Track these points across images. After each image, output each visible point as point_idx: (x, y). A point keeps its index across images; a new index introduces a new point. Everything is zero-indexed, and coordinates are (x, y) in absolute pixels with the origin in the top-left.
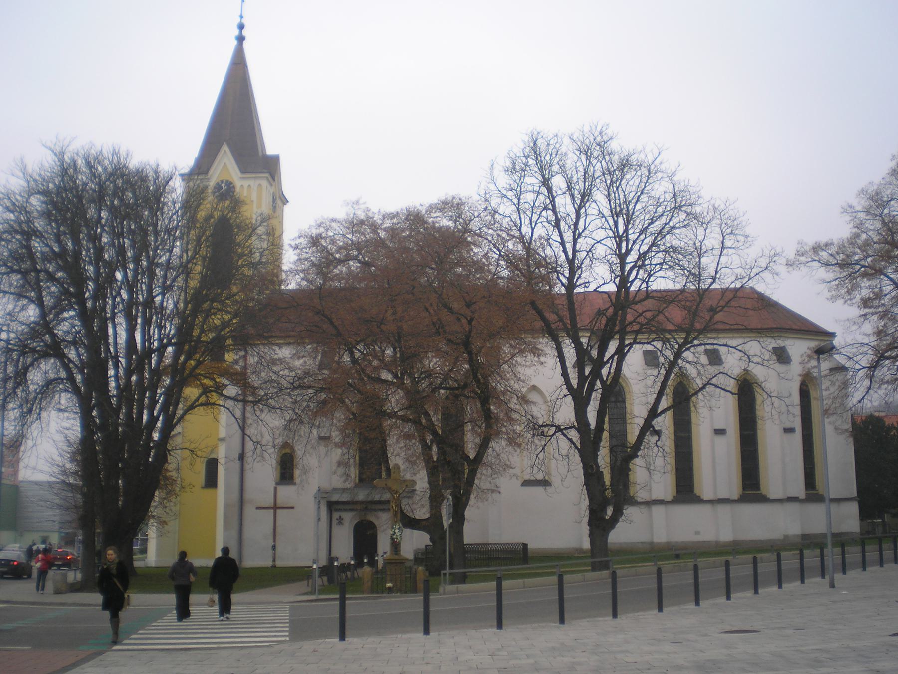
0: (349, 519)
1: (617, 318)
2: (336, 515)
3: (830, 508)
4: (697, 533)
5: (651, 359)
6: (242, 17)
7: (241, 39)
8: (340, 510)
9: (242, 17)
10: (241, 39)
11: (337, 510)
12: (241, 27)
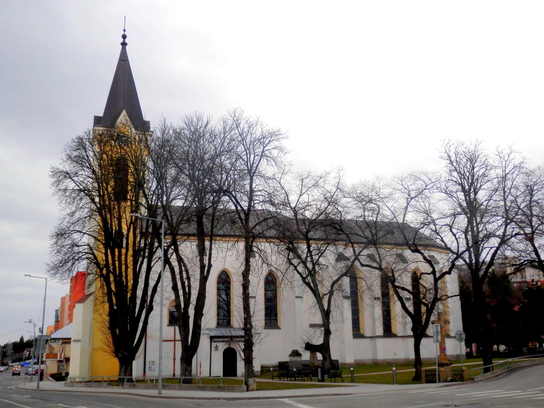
0: (222, 346)
1: (127, 180)
2: (214, 345)
3: (159, 373)
4: (395, 354)
5: (340, 257)
6: (124, 31)
7: (124, 44)
8: (216, 342)
9: (124, 31)
10: (124, 44)
11: (214, 342)
12: (124, 37)
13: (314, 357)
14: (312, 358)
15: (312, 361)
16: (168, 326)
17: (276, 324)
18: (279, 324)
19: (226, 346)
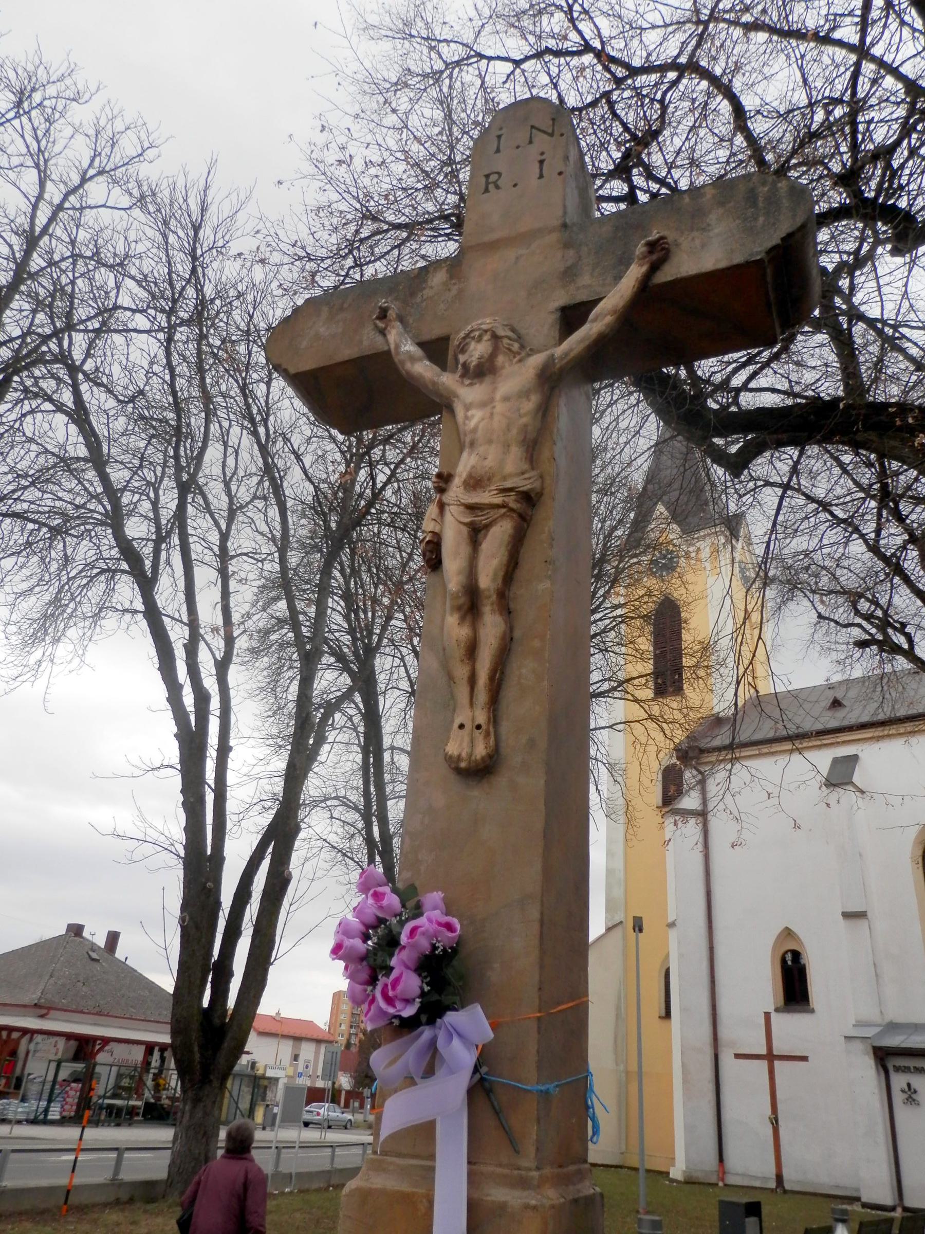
2: (899, 1081)
8: (906, 1070)
11: (897, 1069)
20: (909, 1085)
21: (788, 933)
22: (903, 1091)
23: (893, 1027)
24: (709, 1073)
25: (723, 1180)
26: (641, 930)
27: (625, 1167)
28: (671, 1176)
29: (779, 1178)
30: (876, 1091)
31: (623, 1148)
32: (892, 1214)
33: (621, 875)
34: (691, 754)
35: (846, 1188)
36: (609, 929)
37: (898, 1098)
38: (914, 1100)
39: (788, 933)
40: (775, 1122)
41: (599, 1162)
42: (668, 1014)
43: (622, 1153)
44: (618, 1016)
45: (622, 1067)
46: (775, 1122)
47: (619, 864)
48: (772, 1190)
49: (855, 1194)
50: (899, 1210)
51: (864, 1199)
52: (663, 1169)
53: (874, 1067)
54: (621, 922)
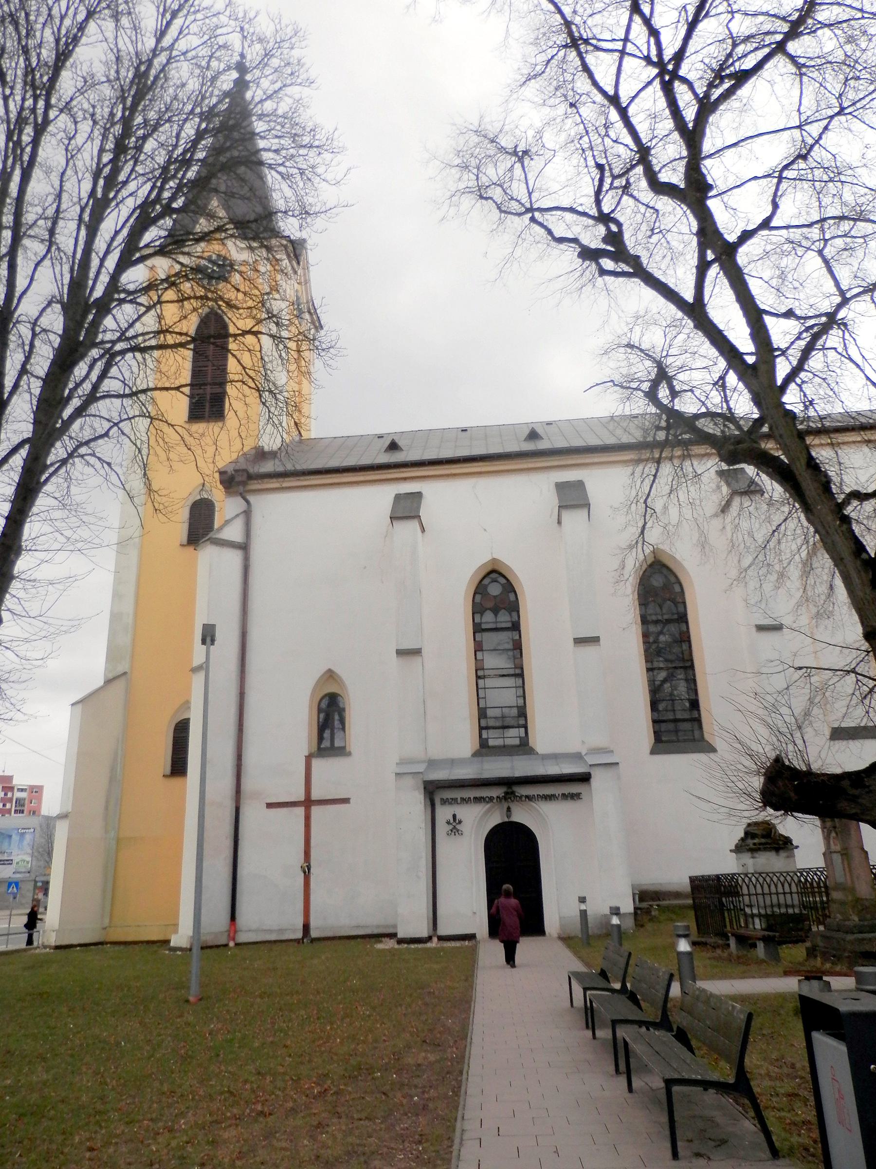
2: (444, 813)
8: (453, 802)
11: (444, 802)
13: (845, 854)
14: (837, 858)
15: (839, 875)
16: (653, 752)
17: (697, 734)
18: (707, 736)
19: (496, 819)
20: (454, 816)
21: (330, 675)
22: (448, 823)
23: (432, 764)
24: (229, 829)
25: (234, 939)
26: (213, 641)
27: (107, 943)
28: (172, 944)
29: (306, 928)
30: (423, 825)
31: (106, 921)
32: (429, 945)
33: (130, 620)
34: (238, 479)
35: (367, 927)
36: (108, 682)
37: (442, 828)
38: (458, 831)
39: (330, 675)
40: (307, 872)
41: (75, 942)
42: (178, 767)
43: (105, 929)
44: (112, 780)
45: (112, 834)
46: (307, 872)
47: (128, 607)
48: (297, 941)
49: (391, 931)
50: (435, 939)
51: (400, 935)
52: (160, 937)
53: (423, 801)
54: (125, 673)
